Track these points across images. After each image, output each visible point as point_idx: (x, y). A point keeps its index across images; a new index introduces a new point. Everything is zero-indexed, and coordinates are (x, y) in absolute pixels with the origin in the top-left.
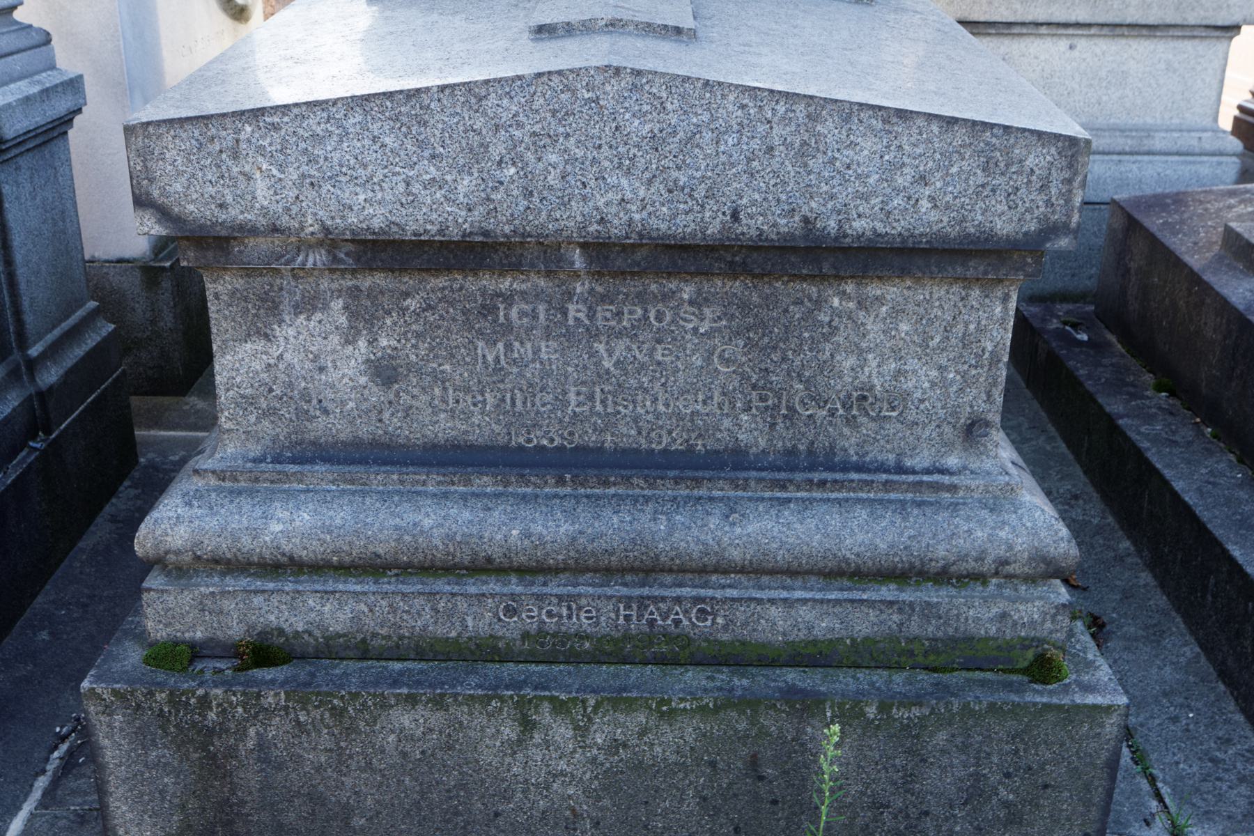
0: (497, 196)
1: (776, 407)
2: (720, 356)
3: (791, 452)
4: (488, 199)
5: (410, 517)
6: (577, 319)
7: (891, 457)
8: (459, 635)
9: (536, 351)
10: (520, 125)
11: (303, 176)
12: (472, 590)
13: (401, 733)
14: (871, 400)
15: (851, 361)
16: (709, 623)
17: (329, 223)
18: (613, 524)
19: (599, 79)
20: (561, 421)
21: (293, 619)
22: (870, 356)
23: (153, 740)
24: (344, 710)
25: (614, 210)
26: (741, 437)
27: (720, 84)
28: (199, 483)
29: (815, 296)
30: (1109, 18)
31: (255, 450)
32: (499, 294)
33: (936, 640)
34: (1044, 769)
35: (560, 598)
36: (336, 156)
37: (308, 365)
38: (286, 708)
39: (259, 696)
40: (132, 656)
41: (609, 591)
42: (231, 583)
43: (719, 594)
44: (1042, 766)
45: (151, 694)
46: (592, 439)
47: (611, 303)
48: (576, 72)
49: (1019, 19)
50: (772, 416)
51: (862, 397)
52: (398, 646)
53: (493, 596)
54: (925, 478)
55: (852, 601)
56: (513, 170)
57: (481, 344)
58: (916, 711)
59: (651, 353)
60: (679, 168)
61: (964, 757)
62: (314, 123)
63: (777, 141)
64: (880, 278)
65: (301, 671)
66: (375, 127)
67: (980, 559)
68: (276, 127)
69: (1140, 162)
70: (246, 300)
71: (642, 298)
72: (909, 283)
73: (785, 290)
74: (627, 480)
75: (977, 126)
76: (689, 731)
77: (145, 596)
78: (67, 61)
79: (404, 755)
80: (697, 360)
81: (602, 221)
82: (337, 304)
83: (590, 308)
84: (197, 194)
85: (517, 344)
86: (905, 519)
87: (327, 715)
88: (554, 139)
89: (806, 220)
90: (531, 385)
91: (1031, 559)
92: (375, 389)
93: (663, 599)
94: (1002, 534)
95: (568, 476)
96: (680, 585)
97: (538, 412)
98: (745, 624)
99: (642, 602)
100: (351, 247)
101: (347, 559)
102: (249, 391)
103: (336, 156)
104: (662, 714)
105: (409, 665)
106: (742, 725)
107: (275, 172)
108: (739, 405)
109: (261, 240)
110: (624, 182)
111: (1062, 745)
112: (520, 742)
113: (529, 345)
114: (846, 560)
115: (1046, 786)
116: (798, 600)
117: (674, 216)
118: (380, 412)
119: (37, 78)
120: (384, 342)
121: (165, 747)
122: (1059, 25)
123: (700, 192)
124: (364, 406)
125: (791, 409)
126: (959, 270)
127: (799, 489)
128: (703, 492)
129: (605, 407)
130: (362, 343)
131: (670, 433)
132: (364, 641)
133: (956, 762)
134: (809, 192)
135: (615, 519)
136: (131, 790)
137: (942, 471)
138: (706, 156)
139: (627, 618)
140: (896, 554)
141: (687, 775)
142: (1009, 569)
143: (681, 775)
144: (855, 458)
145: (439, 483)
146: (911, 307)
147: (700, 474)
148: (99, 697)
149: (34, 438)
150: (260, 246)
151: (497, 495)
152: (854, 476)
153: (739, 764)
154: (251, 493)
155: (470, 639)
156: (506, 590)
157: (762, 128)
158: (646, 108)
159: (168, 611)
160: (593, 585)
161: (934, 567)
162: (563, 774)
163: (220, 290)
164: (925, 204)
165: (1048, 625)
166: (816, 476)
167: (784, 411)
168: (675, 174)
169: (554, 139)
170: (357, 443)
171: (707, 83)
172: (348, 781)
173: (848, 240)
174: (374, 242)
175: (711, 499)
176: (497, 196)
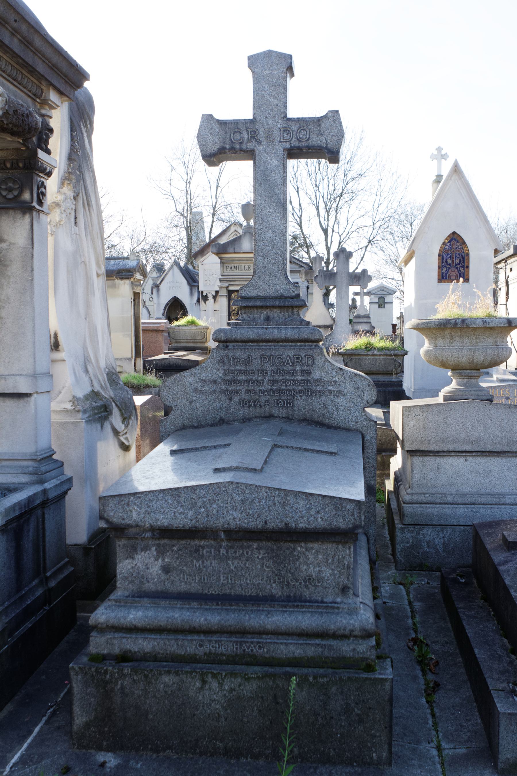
0: (199, 517)
1: (283, 582)
2: (266, 565)
3: (289, 596)
4: (197, 518)
5: (171, 614)
6: (223, 554)
7: (320, 598)
8: (185, 654)
9: (211, 563)
10: (205, 497)
11: (146, 511)
12: (189, 638)
13: (166, 685)
14: (312, 580)
15: (305, 567)
16: (262, 651)
17: (152, 524)
18: (232, 618)
19: (227, 485)
20: (218, 586)
21: (134, 647)
22: (311, 566)
23: (89, 685)
24: (148, 675)
25: (232, 521)
26: (273, 591)
27: (260, 486)
28: (109, 603)
29: (293, 547)
30: (480, 449)
31: (127, 593)
32: (200, 546)
33: (334, 658)
34: (368, 701)
35: (216, 641)
36: (155, 506)
37: (144, 567)
38: (130, 674)
39: (122, 670)
40: (85, 659)
41: (231, 639)
42: (116, 635)
43: (265, 641)
44: (368, 700)
45: (90, 668)
46: (228, 591)
47: (233, 549)
48: (221, 483)
49: (441, 449)
50: (282, 585)
51: (309, 579)
52: (166, 657)
53: (195, 640)
54: (330, 605)
55: (306, 644)
56: (203, 510)
57: (195, 561)
58: (325, 679)
59: (245, 564)
60: (249, 509)
61: (342, 697)
62: (150, 497)
63: (276, 502)
64: (311, 541)
65: (136, 664)
66: (166, 498)
67: (345, 629)
68: (140, 498)
69: (500, 508)
70: (127, 547)
71: (242, 547)
72: (320, 543)
73: (284, 545)
74: (237, 604)
75: (331, 498)
76: (254, 686)
77: (91, 638)
78: (68, 472)
79: (166, 692)
80: (259, 567)
81: (228, 524)
82: (154, 549)
83: (227, 550)
84: (116, 515)
85: (205, 561)
86: (321, 617)
87: (143, 677)
88: (215, 501)
89: (286, 524)
90: (209, 574)
91: (360, 630)
92: (163, 575)
93: (248, 642)
94: (351, 622)
95: (220, 603)
96: (253, 638)
97: (211, 583)
98: (273, 651)
99: (241, 643)
100: (158, 531)
101: (152, 627)
102: (126, 575)
103: (155, 506)
104: (246, 679)
105: (169, 663)
106: (271, 683)
107: (138, 510)
108: (272, 581)
109: (133, 529)
110: (234, 513)
111: (373, 693)
112: (202, 688)
113: (209, 562)
114: (303, 630)
115: (370, 708)
116: (289, 643)
117: (248, 523)
118: (165, 582)
119: (59, 478)
120: (166, 560)
121: (93, 687)
122: (459, 452)
123: (256, 516)
124: (160, 580)
125: (288, 582)
126: (333, 539)
127: (290, 607)
128: (261, 608)
129: (232, 581)
130: (160, 560)
131: (251, 590)
132: (155, 655)
133: (340, 698)
134: (286, 516)
135: (233, 616)
136: (81, 703)
137: (335, 603)
138: (257, 506)
139: (237, 648)
140: (318, 628)
141: (254, 701)
142: (354, 633)
143: (252, 701)
144: (308, 599)
145: (181, 604)
146: (322, 550)
147: (260, 602)
148: (75, 669)
149: (45, 606)
150: (133, 530)
151: (198, 608)
152: (308, 604)
153: (271, 698)
154: (125, 606)
155: (188, 655)
156: (200, 638)
157: (272, 498)
158: (240, 493)
159: (98, 644)
160: (226, 637)
161: (331, 632)
162: (215, 700)
163: (120, 544)
164: (319, 520)
165: (369, 653)
166: (296, 604)
167: (286, 583)
168: (248, 511)
169: (215, 501)
170: (157, 592)
171: (256, 486)
172: (148, 701)
173: (298, 530)
174: (165, 530)
175: (263, 610)
176: (199, 517)
